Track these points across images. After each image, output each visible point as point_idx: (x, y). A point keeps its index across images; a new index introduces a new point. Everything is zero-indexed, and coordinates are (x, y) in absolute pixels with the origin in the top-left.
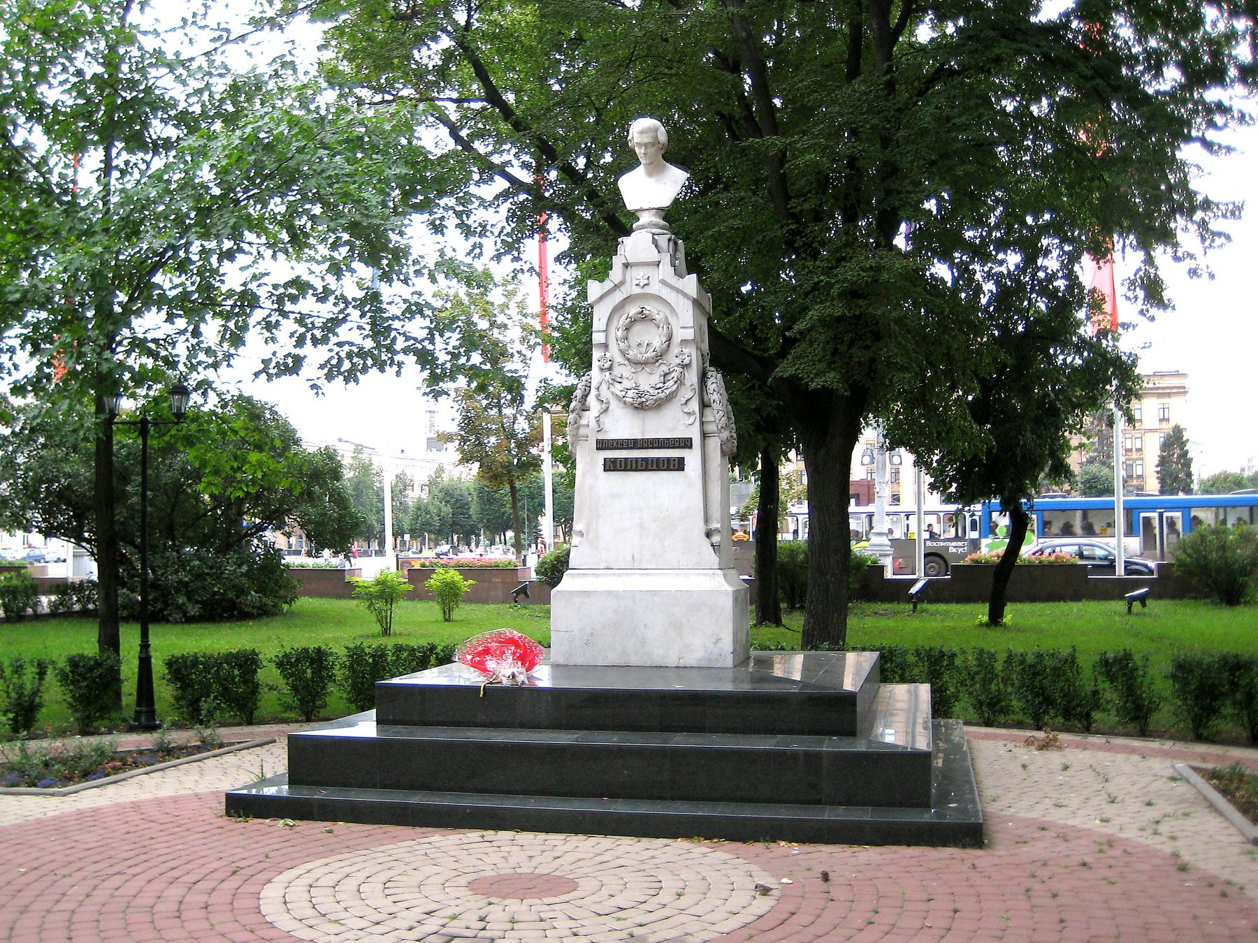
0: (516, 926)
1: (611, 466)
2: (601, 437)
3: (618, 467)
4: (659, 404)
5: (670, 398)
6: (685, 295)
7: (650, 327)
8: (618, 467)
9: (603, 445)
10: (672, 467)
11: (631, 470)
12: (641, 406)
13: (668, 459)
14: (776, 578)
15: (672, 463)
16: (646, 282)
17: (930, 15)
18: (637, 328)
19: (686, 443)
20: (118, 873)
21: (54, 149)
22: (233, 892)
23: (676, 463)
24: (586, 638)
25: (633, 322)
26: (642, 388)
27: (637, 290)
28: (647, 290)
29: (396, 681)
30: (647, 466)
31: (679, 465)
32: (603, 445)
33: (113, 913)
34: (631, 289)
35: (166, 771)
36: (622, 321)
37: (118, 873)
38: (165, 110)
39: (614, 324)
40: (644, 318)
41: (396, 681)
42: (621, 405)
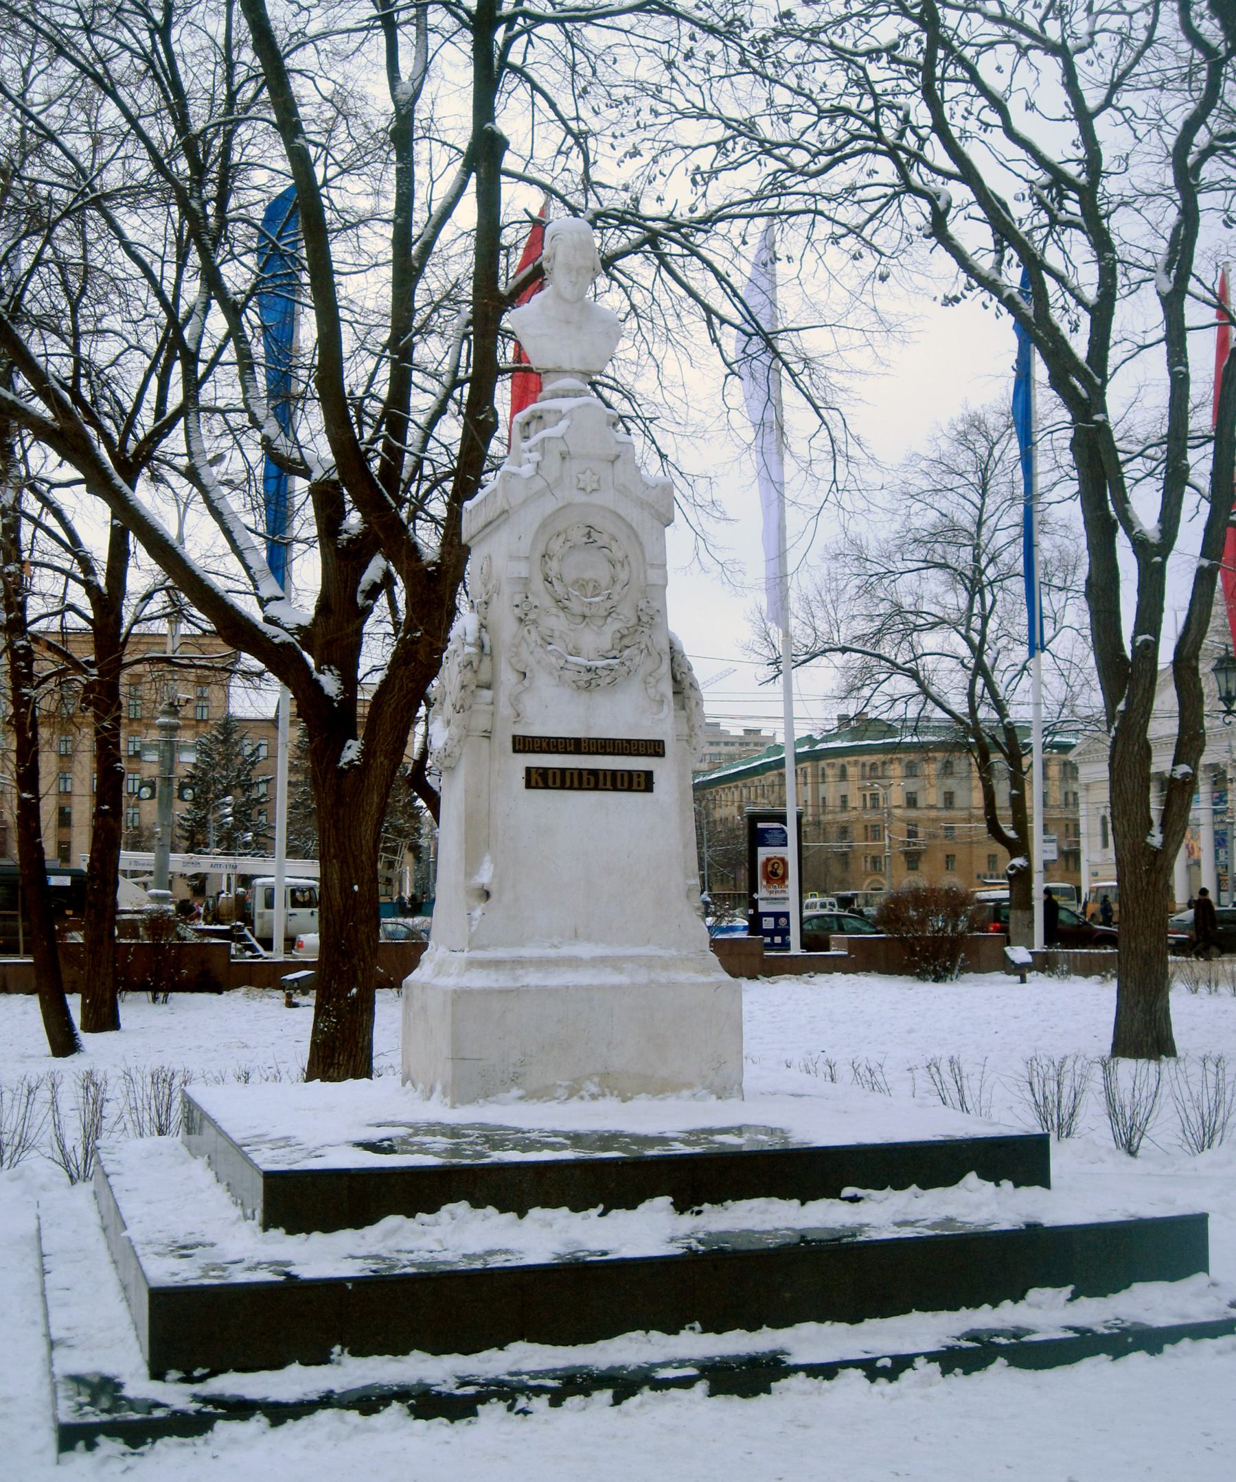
1: (538, 779)
3: (550, 783)
8: (576, 784)
9: (523, 744)
10: (585, 785)
11: (571, 788)
13: (630, 773)
14: (214, 1277)
15: (635, 780)
16: (595, 486)
17: (1007, 949)
19: (655, 748)
21: (231, 417)
23: (642, 780)
24: (511, 1069)
30: (597, 783)
31: (644, 782)
32: (523, 744)
35: (40, 1298)
38: (281, 350)
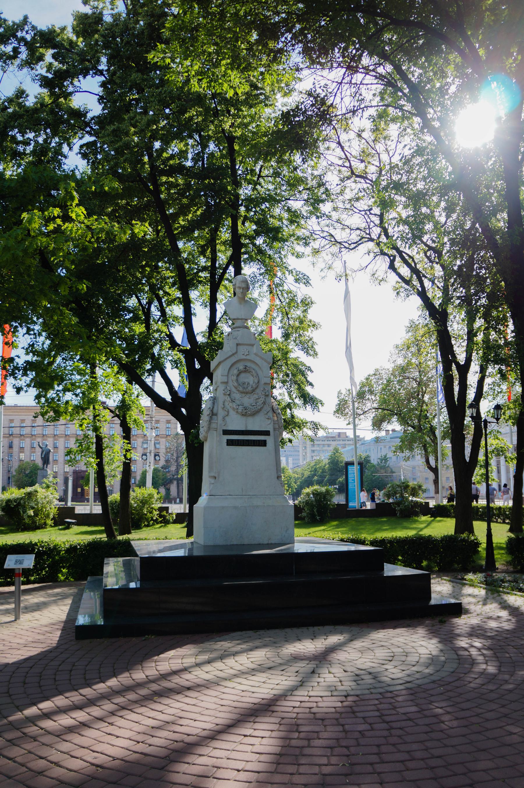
0: (375, 750)
1: (230, 443)
2: (225, 428)
4: (254, 414)
5: (260, 410)
6: (266, 361)
7: (248, 375)
12: (246, 413)
18: (243, 375)
20: (463, 710)
22: (11, 673)
25: (240, 373)
26: (245, 405)
27: (244, 357)
28: (248, 357)
29: (456, 399)
31: (263, 443)
32: (226, 432)
33: (97, 752)
34: (240, 356)
36: (236, 372)
37: (463, 710)
39: (231, 372)
40: (246, 370)
41: (456, 399)
42: (235, 413)
